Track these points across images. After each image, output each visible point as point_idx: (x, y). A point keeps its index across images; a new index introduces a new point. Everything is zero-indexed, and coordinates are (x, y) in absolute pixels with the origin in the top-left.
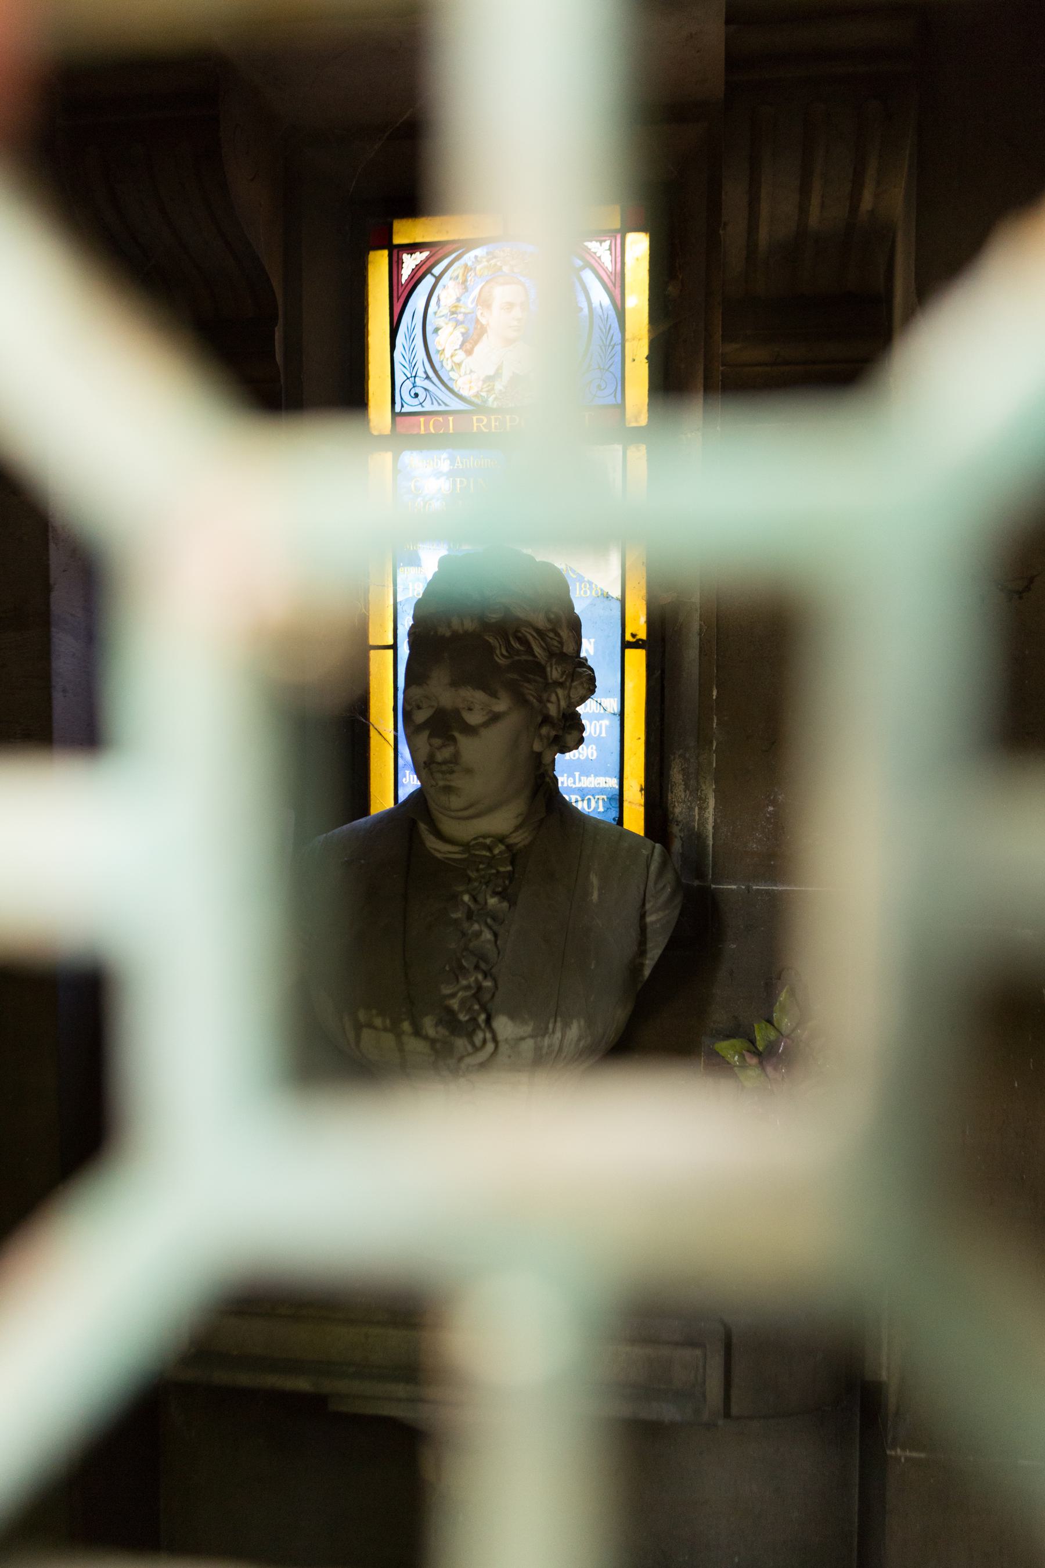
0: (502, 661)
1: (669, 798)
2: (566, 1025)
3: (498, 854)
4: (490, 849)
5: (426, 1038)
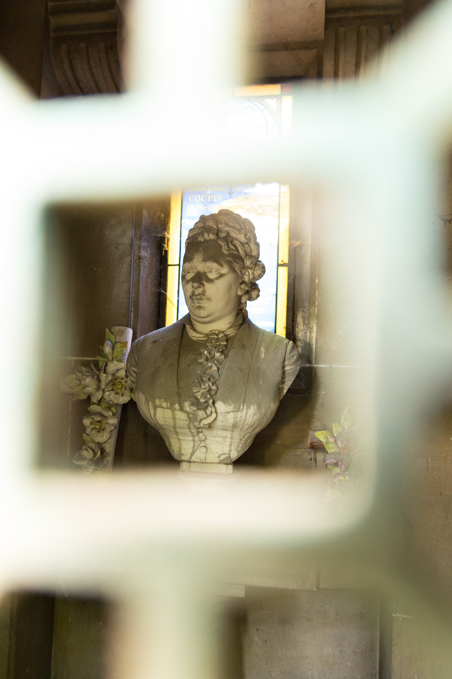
0: (225, 252)
1: (296, 330)
2: (248, 407)
3: (220, 338)
4: (217, 335)
5: (186, 412)
